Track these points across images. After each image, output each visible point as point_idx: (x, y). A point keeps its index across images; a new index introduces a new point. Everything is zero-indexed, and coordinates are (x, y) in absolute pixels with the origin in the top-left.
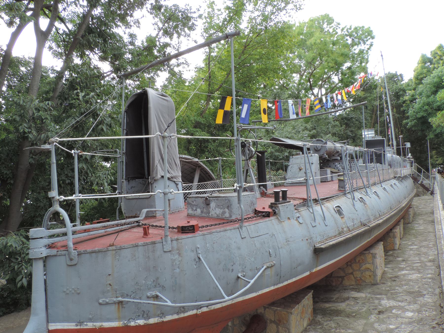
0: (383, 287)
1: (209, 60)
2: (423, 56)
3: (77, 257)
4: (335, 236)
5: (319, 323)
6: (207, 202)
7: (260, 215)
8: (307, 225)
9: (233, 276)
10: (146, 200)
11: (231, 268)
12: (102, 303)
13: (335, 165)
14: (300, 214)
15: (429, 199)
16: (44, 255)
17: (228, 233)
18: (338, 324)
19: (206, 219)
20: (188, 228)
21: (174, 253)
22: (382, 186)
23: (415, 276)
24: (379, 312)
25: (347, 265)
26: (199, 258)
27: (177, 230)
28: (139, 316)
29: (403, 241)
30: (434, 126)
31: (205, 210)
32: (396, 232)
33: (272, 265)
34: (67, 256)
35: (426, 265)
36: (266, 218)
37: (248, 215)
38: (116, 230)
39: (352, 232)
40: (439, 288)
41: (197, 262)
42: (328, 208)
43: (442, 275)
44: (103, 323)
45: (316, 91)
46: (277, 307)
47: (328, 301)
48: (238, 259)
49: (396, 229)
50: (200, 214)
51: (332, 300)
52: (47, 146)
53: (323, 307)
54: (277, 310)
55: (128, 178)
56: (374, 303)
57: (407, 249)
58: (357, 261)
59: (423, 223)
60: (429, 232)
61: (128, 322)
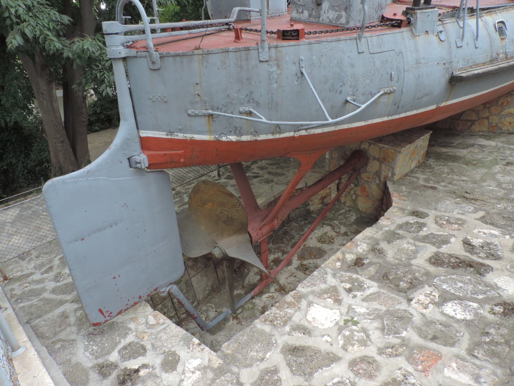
3: (159, 60)
4: (484, 64)
5: (430, 167)
7: (388, 23)
8: (450, 43)
9: (340, 99)
12: (192, 115)
14: (444, 28)
16: (123, 55)
17: (342, 45)
18: (452, 169)
19: (315, 25)
21: (271, 63)
25: (485, 108)
26: (302, 73)
27: (276, 35)
28: (231, 131)
31: (314, 13)
33: (391, 91)
36: (395, 29)
37: (372, 23)
39: (510, 61)
41: (299, 77)
42: (486, 24)
47: (446, 146)
48: (350, 79)
51: (453, 145)
53: (438, 151)
54: (384, 147)
56: (505, 153)
58: (500, 103)
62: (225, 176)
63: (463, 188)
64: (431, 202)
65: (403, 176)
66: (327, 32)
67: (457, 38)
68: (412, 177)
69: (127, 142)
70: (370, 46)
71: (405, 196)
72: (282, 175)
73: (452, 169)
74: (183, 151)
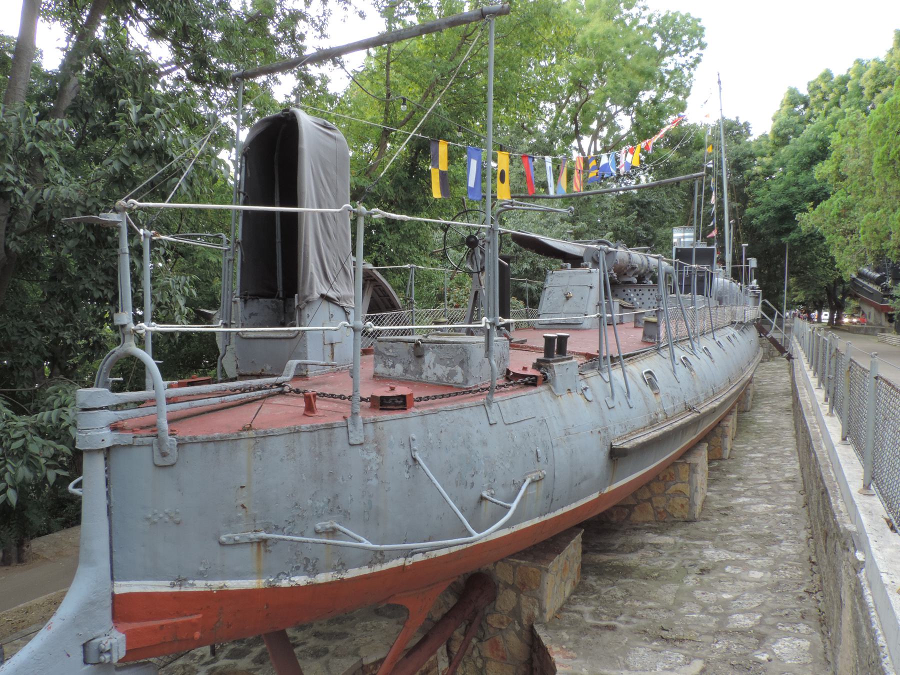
0: (705, 526)
1: (388, 58)
2: (792, 92)
3: (175, 449)
6: (418, 351)
7: (519, 381)
8: (599, 403)
9: (473, 496)
10: (287, 342)
11: (470, 480)
13: (626, 293)
14: (587, 383)
15: (779, 368)
16: (107, 444)
17: (467, 414)
18: (627, 591)
19: (415, 384)
20: (393, 401)
21: (368, 447)
22: (714, 339)
23: (762, 507)
24: (702, 570)
26: (415, 460)
27: (369, 403)
28: (298, 568)
29: (737, 444)
30: (803, 230)
31: (412, 368)
32: (727, 426)
34: (155, 448)
35: (780, 489)
38: (242, 399)
40: (805, 529)
43: (833, 505)
44: (227, 581)
45: (586, 141)
46: (520, 559)
49: (728, 421)
50: (401, 375)
51: (612, 548)
52: (112, 217)
53: (596, 561)
54: (519, 564)
55: (246, 295)
56: (691, 554)
57: (745, 459)
59: (770, 412)
60: (783, 429)
61: (276, 580)
62: (226, 652)
63: (654, 621)
64: (615, 655)
65: (556, 612)
66: (443, 396)
67: (606, 397)
68: (570, 611)
69: (87, 609)
70: (503, 414)
71: (571, 649)
72: (342, 635)
73: (627, 591)
74: (200, 616)
